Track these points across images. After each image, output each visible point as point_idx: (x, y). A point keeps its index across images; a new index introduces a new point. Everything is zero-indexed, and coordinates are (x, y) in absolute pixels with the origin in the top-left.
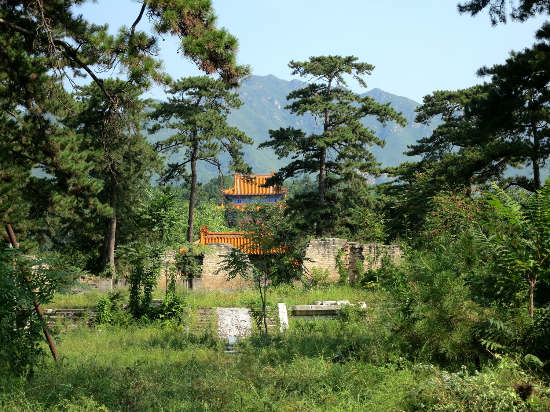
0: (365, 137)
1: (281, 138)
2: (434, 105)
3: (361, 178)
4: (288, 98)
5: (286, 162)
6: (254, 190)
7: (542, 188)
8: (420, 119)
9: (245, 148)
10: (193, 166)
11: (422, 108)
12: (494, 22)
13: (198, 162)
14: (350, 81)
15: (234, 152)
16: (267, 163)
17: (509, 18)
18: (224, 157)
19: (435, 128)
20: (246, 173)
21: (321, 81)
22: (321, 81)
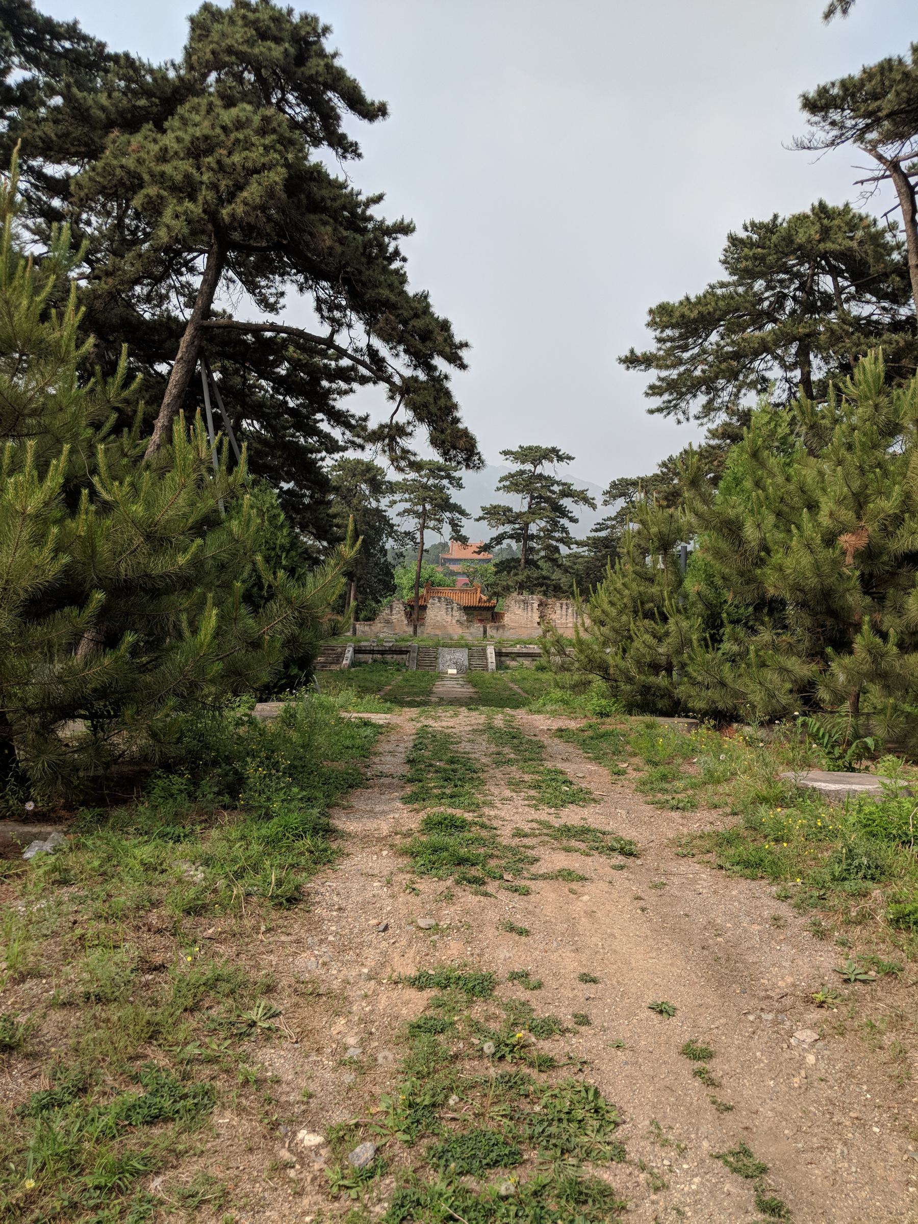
0: (563, 512)
1: (494, 513)
2: (620, 488)
3: (343, 607)
4: (500, 481)
5: (495, 533)
6: (468, 554)
7: (706, 524)
8: (606, 503)
9: (464, 521)
10: (422, 534)
11: (608, 492)
12: (679, 422)
13: (426, 531)
14: (547, 468)
15: (455, 525)
16: (479, 532)
17: (692, 419)
18: (447, 529)
19: (619, 509)
20: (463, 540)
21: (528, 467)
22: (528, 467)
